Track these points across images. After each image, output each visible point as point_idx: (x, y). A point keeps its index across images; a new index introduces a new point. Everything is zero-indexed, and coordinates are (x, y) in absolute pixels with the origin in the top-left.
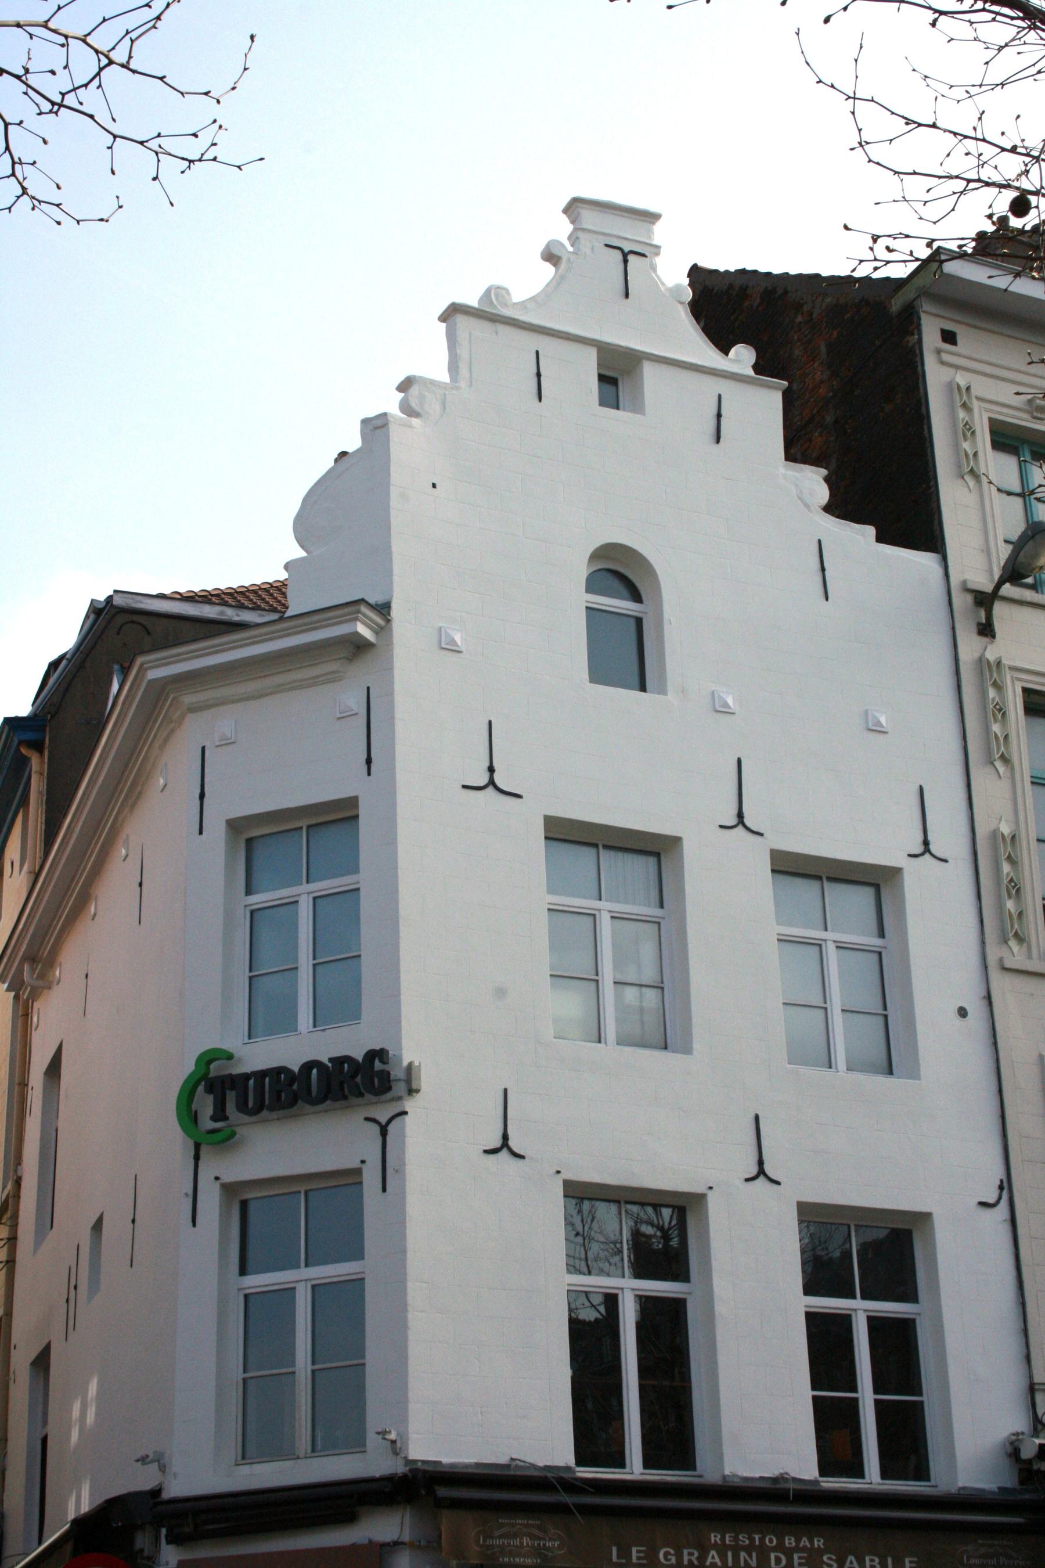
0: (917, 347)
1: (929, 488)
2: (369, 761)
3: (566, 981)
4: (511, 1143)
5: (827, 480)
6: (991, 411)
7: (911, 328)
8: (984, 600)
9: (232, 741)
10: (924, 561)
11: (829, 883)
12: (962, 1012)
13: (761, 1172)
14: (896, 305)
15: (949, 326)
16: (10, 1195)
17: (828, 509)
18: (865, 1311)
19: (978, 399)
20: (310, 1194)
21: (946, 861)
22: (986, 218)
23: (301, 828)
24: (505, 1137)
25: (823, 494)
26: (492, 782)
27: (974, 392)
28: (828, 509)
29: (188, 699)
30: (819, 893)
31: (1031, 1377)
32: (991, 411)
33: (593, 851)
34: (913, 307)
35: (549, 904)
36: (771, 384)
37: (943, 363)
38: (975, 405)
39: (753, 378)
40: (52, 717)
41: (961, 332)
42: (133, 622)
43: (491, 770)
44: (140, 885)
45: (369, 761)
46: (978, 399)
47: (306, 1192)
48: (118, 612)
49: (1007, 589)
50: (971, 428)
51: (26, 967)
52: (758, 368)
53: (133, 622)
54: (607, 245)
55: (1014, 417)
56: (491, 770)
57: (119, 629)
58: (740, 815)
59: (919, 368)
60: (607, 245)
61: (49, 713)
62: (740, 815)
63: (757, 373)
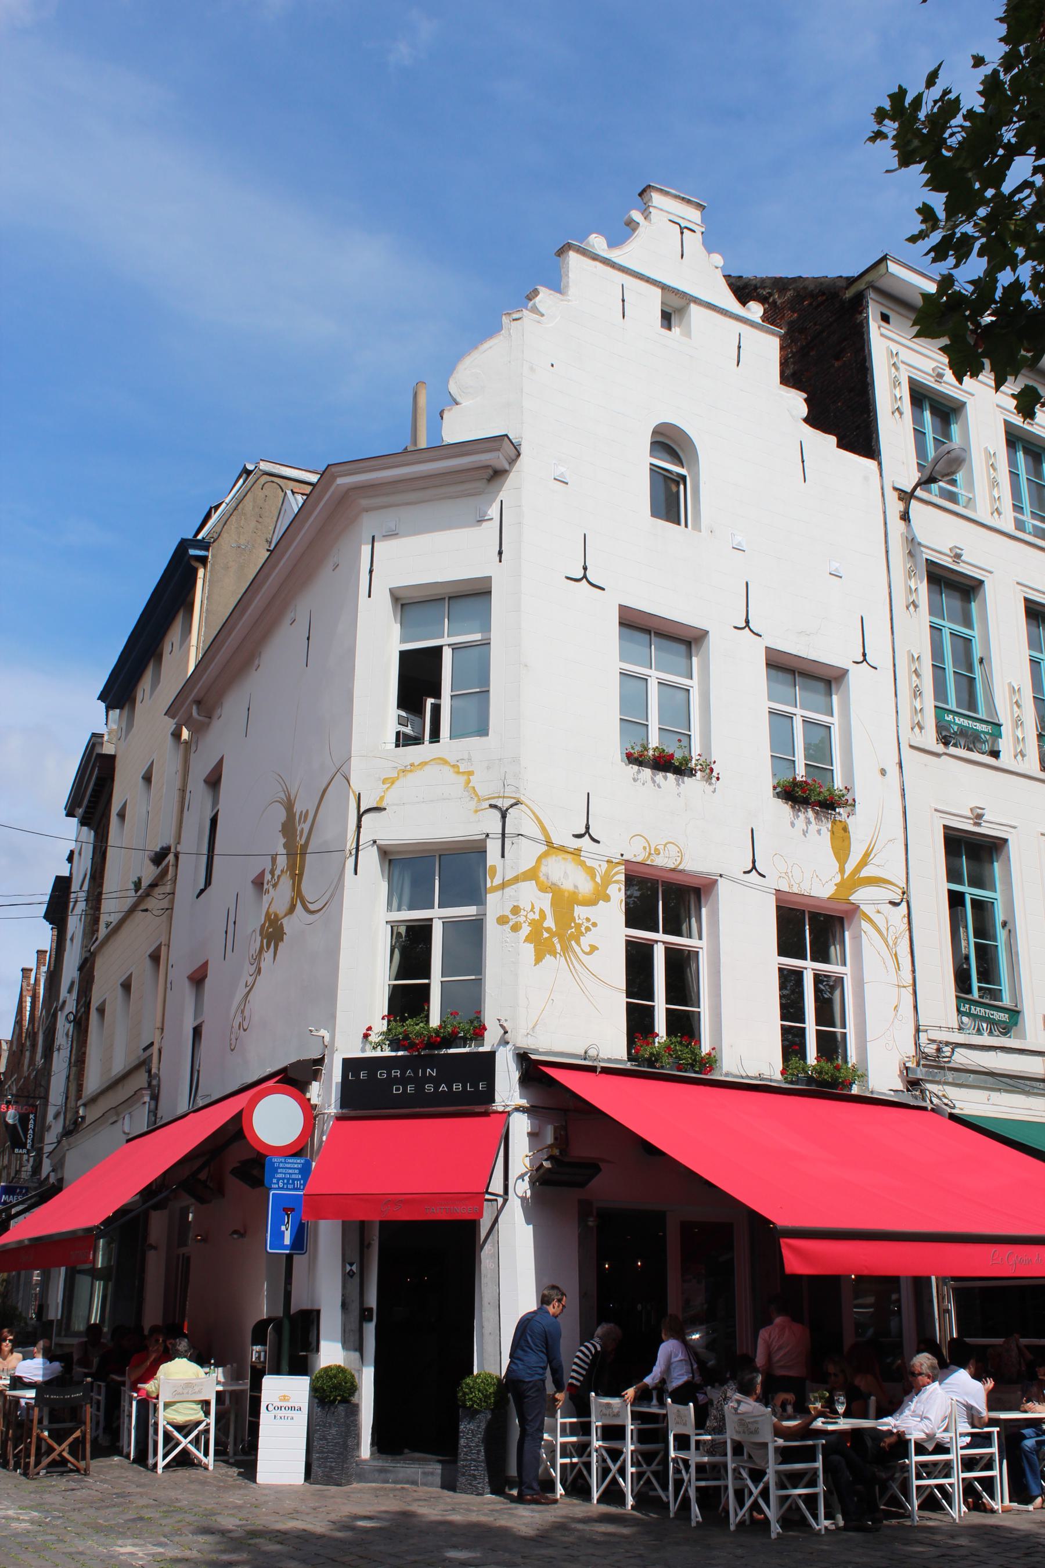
0: (865, 321)
1: (869, 416)
2: (500, 553)
3: (628, 722)
4: (591, 831)
5: (806, 400)
6: (910, 372)
7: (860, 309)
8: (906, 496)
9: (396, 532)
10: (870, 464)
11: (800, 678)
12: (883, 772)
13: (754, 867)
14: (849, 294)
15: (886, 311)
16: (171, 864)
17: (806, 420)
18: (813, 969)
19: (903, 362)
20: (442, 857)
21: (876, 668)
22: (907, 242)
23: (445, 598)
24: (587, 828)
25: (804, 410)
26: (585, 577)
27: (901, 357)
28: (806, 420)
29: (364, 502)
30: (793, 680)
31: (917, 1020)
32: (910, 372)
33: (648, 637)
34: (863, 295)
35: (620, 669)
36: (775, 332)
37: (882, 335)
38: (902, 366)
39: (760, 324)
40: (214, 541)
41: (893, 317)
42: (273, 482)
43: (585, 568)
44: (308, 639)
45: (500, 553)
46: (903, 362)
47: (440, 856)
48: (264, 474)
49: (919, 492)
50: (898, 380)
51: (194, 707)
52: (765, 318)
53: (273, 482)
54: (670, 221)
55: (920, 377)
56: (585, 568)
57: (263, 486)
58: (747, 622)
59: (865, 336)
60: (670, 221)
61: (212, 538)
62: (747, 622)
63: (763, 321)
